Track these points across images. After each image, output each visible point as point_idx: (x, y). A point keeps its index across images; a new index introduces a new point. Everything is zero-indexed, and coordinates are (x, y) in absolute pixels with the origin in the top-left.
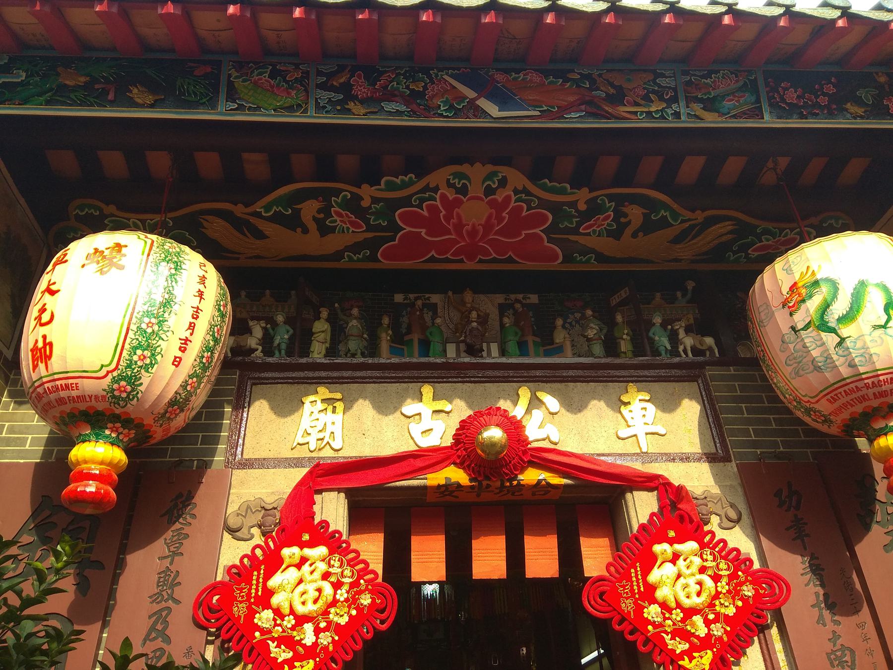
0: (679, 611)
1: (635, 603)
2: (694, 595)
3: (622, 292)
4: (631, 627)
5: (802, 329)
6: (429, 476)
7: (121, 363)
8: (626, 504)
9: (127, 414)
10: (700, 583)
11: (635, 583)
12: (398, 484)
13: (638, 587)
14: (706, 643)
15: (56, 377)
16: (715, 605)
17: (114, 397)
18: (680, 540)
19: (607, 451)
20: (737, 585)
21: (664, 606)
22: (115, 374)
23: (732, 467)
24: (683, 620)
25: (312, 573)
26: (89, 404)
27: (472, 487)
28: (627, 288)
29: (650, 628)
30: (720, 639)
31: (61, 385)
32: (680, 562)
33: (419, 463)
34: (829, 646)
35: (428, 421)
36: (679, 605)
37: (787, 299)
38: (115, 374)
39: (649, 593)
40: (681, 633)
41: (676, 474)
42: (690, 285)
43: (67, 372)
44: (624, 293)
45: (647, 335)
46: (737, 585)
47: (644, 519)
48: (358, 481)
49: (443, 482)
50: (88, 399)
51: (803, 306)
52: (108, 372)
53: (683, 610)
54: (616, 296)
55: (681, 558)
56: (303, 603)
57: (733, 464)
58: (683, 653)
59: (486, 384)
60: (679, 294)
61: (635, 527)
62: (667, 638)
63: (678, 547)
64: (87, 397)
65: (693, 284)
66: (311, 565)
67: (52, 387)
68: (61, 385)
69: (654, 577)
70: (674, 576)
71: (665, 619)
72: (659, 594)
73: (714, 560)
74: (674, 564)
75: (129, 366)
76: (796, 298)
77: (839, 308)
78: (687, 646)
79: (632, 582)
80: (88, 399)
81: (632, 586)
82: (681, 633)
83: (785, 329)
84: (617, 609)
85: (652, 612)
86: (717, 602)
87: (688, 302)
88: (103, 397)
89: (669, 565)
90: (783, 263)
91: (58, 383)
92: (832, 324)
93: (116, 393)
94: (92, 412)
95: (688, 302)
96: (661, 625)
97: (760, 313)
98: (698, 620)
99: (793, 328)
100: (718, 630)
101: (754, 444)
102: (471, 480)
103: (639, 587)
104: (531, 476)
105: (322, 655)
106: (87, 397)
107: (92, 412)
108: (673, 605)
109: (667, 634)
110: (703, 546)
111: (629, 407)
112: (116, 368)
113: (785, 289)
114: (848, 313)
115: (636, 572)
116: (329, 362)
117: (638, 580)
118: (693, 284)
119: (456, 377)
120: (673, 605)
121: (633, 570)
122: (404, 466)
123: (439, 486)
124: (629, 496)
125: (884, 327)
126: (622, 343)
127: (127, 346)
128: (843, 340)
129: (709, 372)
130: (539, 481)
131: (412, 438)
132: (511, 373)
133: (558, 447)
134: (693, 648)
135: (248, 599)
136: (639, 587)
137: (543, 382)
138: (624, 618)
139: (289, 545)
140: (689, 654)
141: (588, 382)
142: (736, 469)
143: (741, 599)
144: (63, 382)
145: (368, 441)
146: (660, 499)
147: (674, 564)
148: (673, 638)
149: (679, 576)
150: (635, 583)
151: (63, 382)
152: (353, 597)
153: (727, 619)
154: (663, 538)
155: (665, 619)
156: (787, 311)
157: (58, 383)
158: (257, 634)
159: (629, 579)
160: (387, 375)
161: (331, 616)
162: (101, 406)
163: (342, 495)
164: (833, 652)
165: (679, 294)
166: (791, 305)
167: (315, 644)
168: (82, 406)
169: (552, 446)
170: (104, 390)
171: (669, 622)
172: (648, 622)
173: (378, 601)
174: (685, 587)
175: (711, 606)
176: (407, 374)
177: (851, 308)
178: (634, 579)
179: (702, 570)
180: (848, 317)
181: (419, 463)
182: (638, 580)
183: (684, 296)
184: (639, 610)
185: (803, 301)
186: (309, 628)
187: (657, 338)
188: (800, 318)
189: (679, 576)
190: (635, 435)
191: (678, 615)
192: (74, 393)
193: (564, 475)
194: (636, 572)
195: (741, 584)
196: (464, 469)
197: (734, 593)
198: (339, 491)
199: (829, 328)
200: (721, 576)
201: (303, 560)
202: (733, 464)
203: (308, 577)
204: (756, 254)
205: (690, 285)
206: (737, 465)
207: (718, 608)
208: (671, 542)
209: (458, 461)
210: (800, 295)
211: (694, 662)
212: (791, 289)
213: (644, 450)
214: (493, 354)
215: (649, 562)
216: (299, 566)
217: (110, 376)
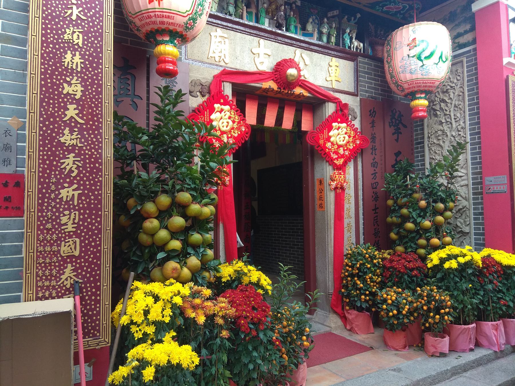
0: (219, 131)
1: (324, 141)
2: (342, 141)
3: (335, 12)
4: (321, 149)
5: (412, 57)
6: (263, 83)
7: (194, 11)
8: (325, 108)
9: (186, 35)
10: (228, 123)
11: (206, 118)
12: (250, 84)
13: (326, 136)
14: (342, 156)
15: (164, 10)
16: (231, 132)
17: (186, 27)
18: (341, 122)
19: (322, 85)
20: (355, 139)
21: (333, 144)
22: (191, 16)
23: (358, 99)
24: (337, 149)
25: (225, 115)
26: (175, 27)
27: (277, 91)
28: (338, 11)
29: (327, 150)
30: (347, 155)
31: (166, 15)
32: (340, 130)
33: (261, 77)
34: (372, 161)
35: (262, 58)
36: (337, 144)
37: (410, 43)
38: (191, 16)
39: (328, 139)
40: (336, 153)
41: (344, 99)
42: (359, 15)
43: (171, 10)
44: (336, 12)
45: (343, 36)
46: (355, 139)
47: (330, 114)
48: (239, 80)
49: (268, 87)
50: (176, 25)
51: (415, 48)
52: (188, 15)
53: (221, 131)
54: (331, 12)
55: (341, 129)
56: (223, 127)
57: (359, 97)
58: (335, 158)
59: (284, 45)
60: (353, 18)
61: (327, 116)
62: (332, 153)
63: (340, 125)
64: (176, 24)
65: (360, 16)
66: (225, 112)
67: (160, 15)
68: (166, 15)
69: (213, 117)
70: (337, 134)
71: (332, 147)
72: (332, 139)
73: (350, 131)
74: (221, 113)
75: (195, 14)
76: (413, 44)
77: (427, 53)
78: (337, 156)
79: (205, 117)
80: (176, 25)
81: (205, 118)
82: (336, 153)
83: (405, 55)
84: (318, 143)
85: (328, 145)
86: (232, 131)
87: (355, 23)
88: (183, 26)
89: (218, 113)
90: (413, 28)
91: (165, 14)
92: (423, 58)
93: (188, 25)
94: (174, 31)
95: (355, 23)
96: (330, 149)
97: (396, 45)
98: (225, 136)
99: (408, 55)
100: (347, 153)
101: (366, 92)
102: (278, 88)
103: (207, 120)
104: (298, 91)
105: (346, 157)
106: (176, 24)
107: (174, 31)
108: (218, 129)
109: (332, 152)
110: (348, 125)
111: (331, 68)
112: (191, 13)
113: (411, 39)
114: (429, 56)
115: (207, 113)
116: (223, 16)
117: (207, 116)
118: (360, 16)
119: (274, 39)
120: (218, 129)
121: (206, 112)
122: (254, 77)
123: (266, 88)
124: (327, 104)
125: (437, 64)
126: (333, 37)
127: (197, 3)
128: (423, 65)
129: (360, 59)
130: (301, 93)
131: (256, 64)
132: (294, 42)
133: (306, 80)
134: (339, 157)
135: (324, 139)
136: (207, 120)
137: (304, 49)
138: (319, 145)
139: (217, 103)
140: (337, 159)
141: (320, 53)
142: (359, 100)
143: (240, 131)
144: (167, 14)
145: (239, 62)
146: (337, 107)
147: (221, 113)
148: (333, 154)
149: (339, 134)
150: (206, 118)
151: (167, 14)
152: (239, 127)
153: (350, 150)
154: (336, 121)
155: (332, 147)
156: (408, 48)
157: (165, 14)
158: (327, 150)
159: (323, 133)
160: (246, 30)
161: (348, 146)
162: (179, 29)
163: (231, 84)
164: (373, 163)
165: (353, 18)
166: (411, 46)
167: (344, 154)
168: (171, 28)
169: (305, 79)
170: (184, 23)
171: (333, 149)
172: (327, 148)
173: (247, 130)
174: (340, 138)
175: (230, 132)
176: (255, 32)
177: (430, 55)
178: (206, 116)
179: (346, 133)
180: (428, 57)
181: (261, 77)
182: (207, 116)
183: (354, 20)
184: (325, 144)
185: (416, 46)
186: (341, 149)
187: (346, 39)
188: (413, 52)
189: (339, 134)
190: (332, 80)
191: (336, 147)
192: (171, 21)
193: (310, 92)
194: (207, 113)
195: (356, 139)
196: (276, 83)
197: (238, 129)
198: (230, 82)
199: (421, 59)
200: (351, 136)
201: (339, 128)
202: (359, 97)
203: (224, 117)
204: (385, 9)
205: (359, 15)
206: (361, 99)
207: (232, 133)
208: (339, 123)
209: (275, 79)
210: (415, 43)
211: (338, 161)
212: (413, 40)
213: (333, 87)
214: (266, 24)
215: (330, 128)
216: (338, 129)
217: (188, 17)
